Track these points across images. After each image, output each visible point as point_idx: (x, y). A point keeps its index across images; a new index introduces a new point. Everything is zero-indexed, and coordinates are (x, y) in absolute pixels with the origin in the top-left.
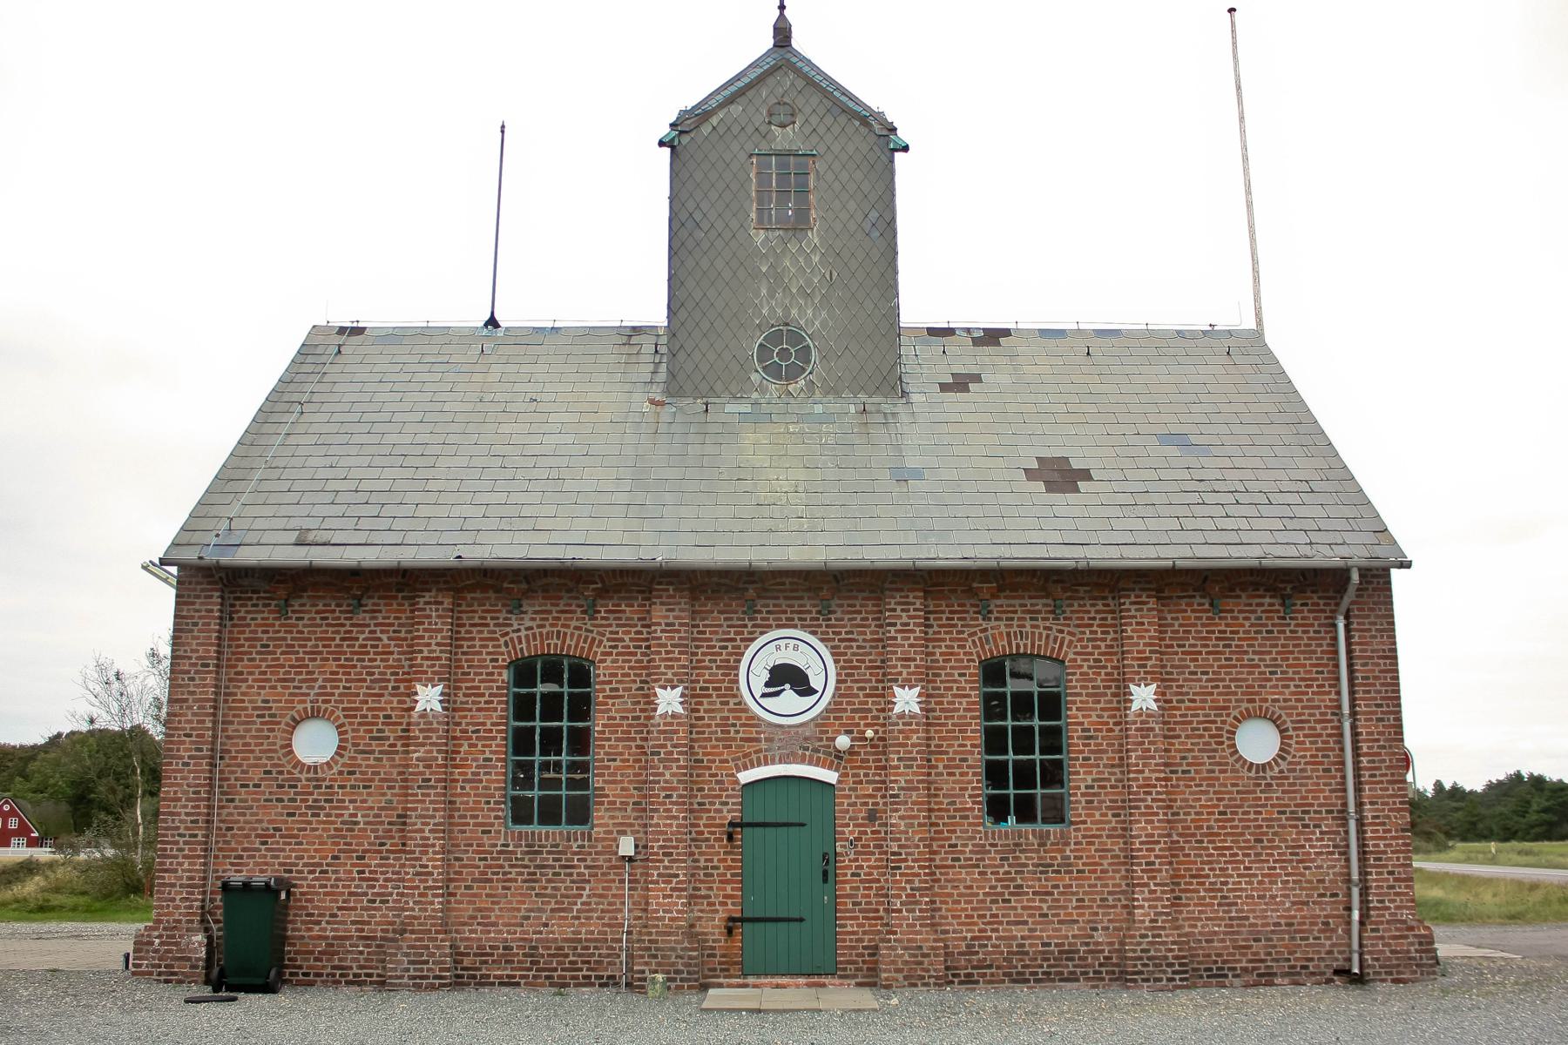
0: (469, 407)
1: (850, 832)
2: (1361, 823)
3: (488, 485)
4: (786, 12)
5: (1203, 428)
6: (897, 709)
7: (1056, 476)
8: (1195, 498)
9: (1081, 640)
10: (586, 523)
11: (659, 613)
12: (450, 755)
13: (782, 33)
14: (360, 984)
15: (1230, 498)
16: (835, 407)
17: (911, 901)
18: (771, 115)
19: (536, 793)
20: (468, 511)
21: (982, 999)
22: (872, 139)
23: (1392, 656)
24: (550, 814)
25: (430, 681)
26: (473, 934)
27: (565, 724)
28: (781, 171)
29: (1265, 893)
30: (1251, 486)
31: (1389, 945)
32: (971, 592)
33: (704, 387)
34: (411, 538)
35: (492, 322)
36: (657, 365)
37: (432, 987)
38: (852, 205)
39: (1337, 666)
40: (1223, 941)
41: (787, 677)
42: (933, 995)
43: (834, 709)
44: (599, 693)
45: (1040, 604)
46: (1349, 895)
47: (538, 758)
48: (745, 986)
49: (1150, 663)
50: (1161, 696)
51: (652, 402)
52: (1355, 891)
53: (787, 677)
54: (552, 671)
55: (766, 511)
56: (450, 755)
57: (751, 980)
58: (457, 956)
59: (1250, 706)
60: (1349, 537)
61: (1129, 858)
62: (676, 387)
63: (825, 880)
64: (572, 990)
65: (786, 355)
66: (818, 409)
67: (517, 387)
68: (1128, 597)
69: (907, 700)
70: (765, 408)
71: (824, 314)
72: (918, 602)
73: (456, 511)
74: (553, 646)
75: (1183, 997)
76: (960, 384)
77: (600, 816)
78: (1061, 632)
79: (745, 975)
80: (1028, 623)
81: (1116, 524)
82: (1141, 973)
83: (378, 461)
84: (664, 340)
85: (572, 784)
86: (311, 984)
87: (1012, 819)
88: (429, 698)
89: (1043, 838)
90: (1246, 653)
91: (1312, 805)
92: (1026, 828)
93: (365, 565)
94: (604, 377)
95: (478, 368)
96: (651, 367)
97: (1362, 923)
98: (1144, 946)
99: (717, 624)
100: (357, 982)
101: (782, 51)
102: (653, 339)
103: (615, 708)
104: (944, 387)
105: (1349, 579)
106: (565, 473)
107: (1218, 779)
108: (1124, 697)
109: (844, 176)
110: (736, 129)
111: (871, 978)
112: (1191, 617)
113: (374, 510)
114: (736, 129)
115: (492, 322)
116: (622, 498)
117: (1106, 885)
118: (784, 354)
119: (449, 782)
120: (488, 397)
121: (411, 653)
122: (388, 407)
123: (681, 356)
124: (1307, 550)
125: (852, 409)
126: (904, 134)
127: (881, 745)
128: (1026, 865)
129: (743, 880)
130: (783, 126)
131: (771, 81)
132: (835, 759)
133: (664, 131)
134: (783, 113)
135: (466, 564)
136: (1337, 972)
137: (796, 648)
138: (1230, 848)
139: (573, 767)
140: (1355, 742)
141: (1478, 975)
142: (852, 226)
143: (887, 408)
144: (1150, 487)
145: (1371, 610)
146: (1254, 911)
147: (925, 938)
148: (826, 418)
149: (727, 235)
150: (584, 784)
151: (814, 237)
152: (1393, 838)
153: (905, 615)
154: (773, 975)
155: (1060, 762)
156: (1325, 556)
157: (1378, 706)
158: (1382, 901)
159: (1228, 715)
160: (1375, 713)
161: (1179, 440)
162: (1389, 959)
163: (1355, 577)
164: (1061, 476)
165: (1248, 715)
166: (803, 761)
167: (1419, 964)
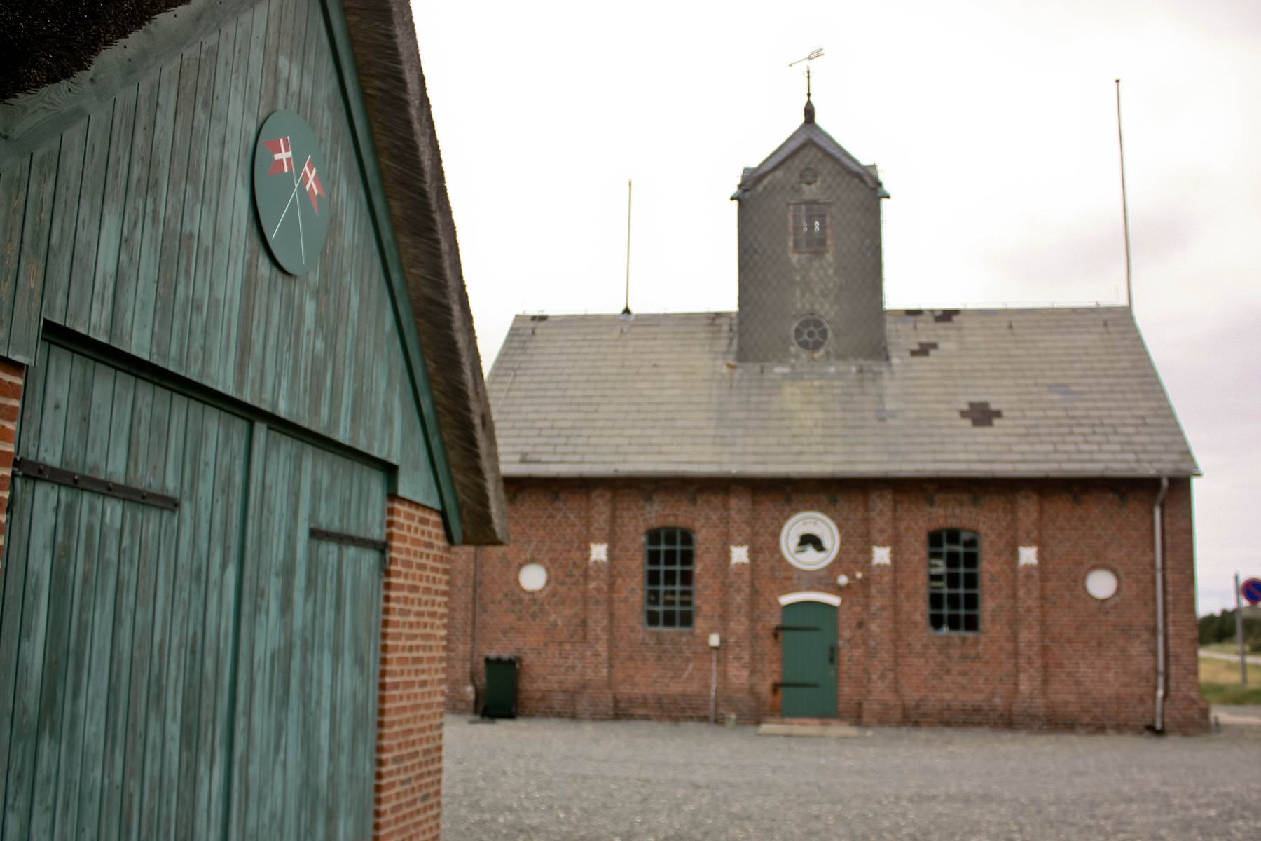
0: (615, 371)
1: (846, 634)
4: (812, 98)
8: (1065, 430)
11: (734, 503)
12: (612, 586)
13: (809, 112)
16: (843, 368)
20: (619, 441)
21: (923, 734)
24: (669, 620)
26: (625, 690)
28: (809, 207)
29: (1099, 677)
30: (1106, 421)
34: (587, 458)
35: (627, 311)
43: (838, 561)
44: (698, 548)
45: (965, 497)
51: (730, 366)
54: (670, 538)
55: (797, 440)
56: (612, 586)
58: (616, 702)
60: (1164, 457)
61: (1016, 654)
62: (743, 355)
63: (832, 660)
65: (812, 335)
66: (832, 369)
67: (646, 356)
69: (882, 555)
70: (799, 369)
74: (671, 521)
75: (1042, 739)
76: (924, 350)
77: (700, 623)
83: (564, 408)
84: (735, 322)
85: (683, 603)
88: (599, 552)
89: (964, 640)
92: (955, 634)
99: (768, 509)
100: (559, 715)
104: (914, 353)
108: (1015, 555)
112: (1060, 509)
113: (563, 440)
115: (627, 311)
116: (711, 432)
118: (811, 334)
119: (611, 602)
121: (588, 525)
124: (1134, 465)
125: (854, 369)
126: (887, 187)
130: (809, 183)
131: (801, 154)
132: (838, 590)
133: (734, 190)
134: (808, 175)
139: (683, 593)
141: (1240, 733)
143: (876, 368)
147: (890, 698)
148: (840, 376)
150: (689, 603)
151: (829, 257)
153: (881, 506)
156: (1148, 469)
161: (1063, 389)
163: (1165, 483)
164: (982, 415)
167: (1193, 723)
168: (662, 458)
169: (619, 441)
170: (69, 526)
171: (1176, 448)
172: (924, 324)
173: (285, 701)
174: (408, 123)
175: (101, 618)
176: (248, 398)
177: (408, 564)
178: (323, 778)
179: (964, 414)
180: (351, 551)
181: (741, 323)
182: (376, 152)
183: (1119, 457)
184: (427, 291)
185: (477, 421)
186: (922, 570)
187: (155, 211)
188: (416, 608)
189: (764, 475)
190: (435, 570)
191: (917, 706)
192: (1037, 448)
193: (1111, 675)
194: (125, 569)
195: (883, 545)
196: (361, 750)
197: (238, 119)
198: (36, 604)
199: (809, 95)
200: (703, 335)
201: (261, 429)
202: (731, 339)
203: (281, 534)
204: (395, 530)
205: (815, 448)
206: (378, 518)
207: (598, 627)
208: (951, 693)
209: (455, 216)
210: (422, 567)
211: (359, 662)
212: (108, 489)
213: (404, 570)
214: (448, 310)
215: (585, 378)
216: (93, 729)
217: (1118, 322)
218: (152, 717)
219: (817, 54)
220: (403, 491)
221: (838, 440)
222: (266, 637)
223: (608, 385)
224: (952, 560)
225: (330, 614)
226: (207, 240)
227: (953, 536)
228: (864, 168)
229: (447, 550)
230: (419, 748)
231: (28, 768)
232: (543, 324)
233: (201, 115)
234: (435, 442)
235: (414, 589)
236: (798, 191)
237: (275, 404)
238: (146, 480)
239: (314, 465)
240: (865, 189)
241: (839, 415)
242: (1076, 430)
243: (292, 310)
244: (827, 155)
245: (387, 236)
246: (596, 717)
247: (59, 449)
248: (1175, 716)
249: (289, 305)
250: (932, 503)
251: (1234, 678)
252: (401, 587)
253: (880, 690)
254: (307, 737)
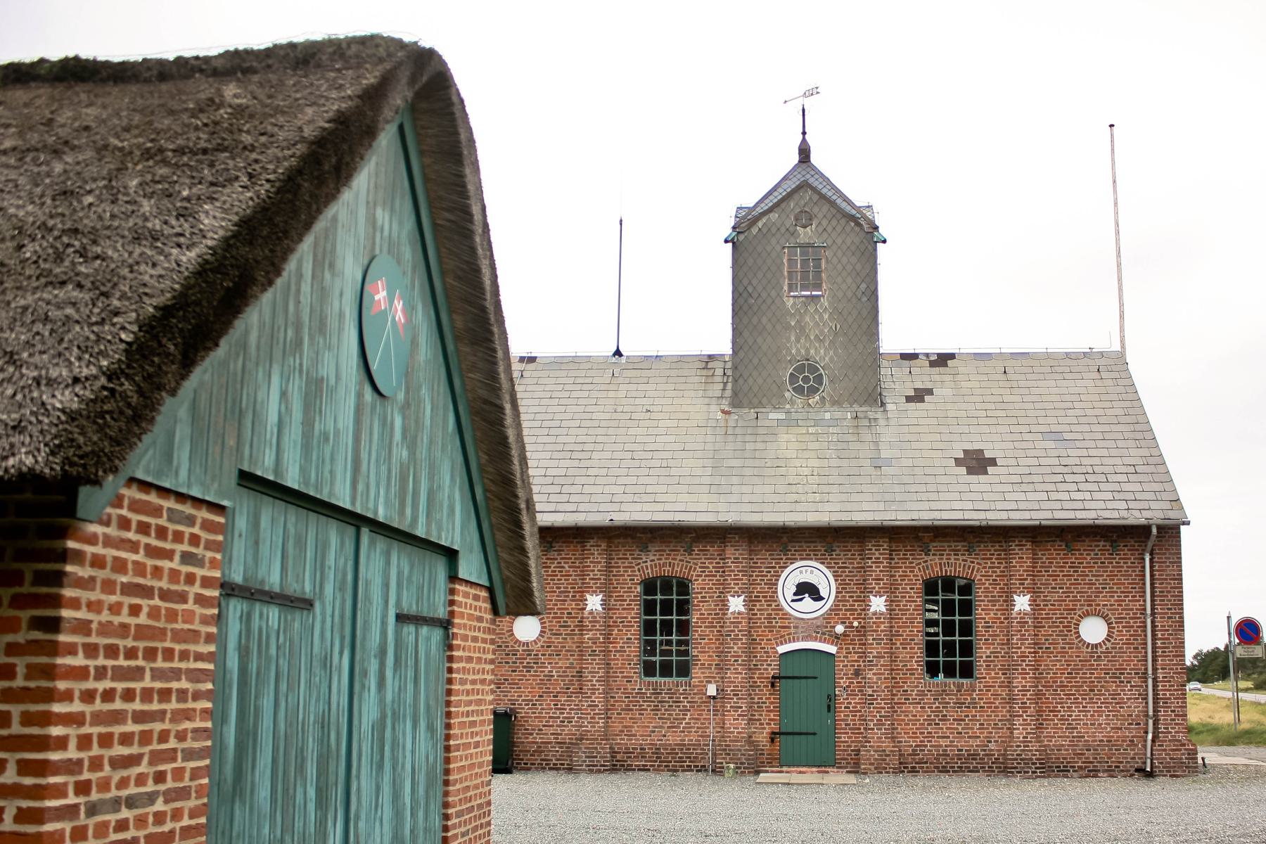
0: (608, 416)
1: (843, 682)
2: (1155, 680)
3: (624, 471)
5: (1074, 428)
6: (872, 610)
7: (974, 463)
8: (1060, 478)
10: (686, 497)
11: (730, 552)
12: (607, 636)
13: (804, 152)
14: (557, 769)
15: (1082, 478)
16: (838, 415)
17: (880, 724)
18: (797, 220)
19: (657, 658)
20: (614, 489)
21: (920, 781)
22: (862, 234)
23: (1179, 579)
24: (666, 670)
26: (622, 740)
27: (674, 617)
28: (802, 250)
29: (1094, 723)
32: (918, 539)
33: (755, 401)
35: (618, 353)
36: (725, 384)
37: (599, 771)
38: (849, 280)
39: (1144, 584)
41: (807, 589)
42: (892, 778)
43: (835, 609)
45: (960, 545)
46: (1147, 724)
47: (658, 638)
50: (1033, 602)
51: (723, 412)
52: (1151, 722)
53: (807, 589)
55: (794, 488)
56: (607, 636)
57: (785, 769)
58: (613, 753)
60: (1154, 505)
61: (1011, 700)
63: (829, 710)
64: (680, 773)
65: (807, 380)
66: (828, 416)
67: (638, 401)
69: (878, 604)
70: (794, 416)
71: (831, 352)
73: (607, 489)
74: (667, 571)
75: (1037, 783)
76: (919, 396)
77: (696, 672)
80: (953, 557)
81: (1008, 497)
83: (556, 455)
84: (729, 365)
85: (679, 653)
86: (529, 769)
87: (941, 675)
88: (594, 602)
89: (959, 687)
92: (951, 680)
93: (556, 525)
94: (692, 394)
95: (612, 387)
96: (721, 386)
97: (1153, 741)
99: (764, 558)
100: (555, 768)
101: (804, 166)
102: (722, 365)
103: (704, 608)
104: (909, 399)
105: (1151, 532)
106: (671, 463)
108: (1010, 603)
109: (844, 260)
110: (774, 230)
111: (855, 769)
113: (557, 489)
114: (774, 230)
115: (618, 353)
116: (707, 480)
118: (806, 379)
119: (607, 652)
120: (620, 409)
121: (583, 575)
122: (557, 417)
123: (741, 381)
124: (1124, 514)
126: (884, 231)
127: (862, 631)
129: (781, 710)
130: (804, 227)
131: (796, 196)
132: (836, 639)
133: (727, 231)
134: (805, 218)
135: (616, 523)
136: (1137, 770)
137: (812, 572)
139: (679, 643)
140: (1153, 631)
141: (1225, 774)
142: (849, 294)
144: (1033, 470)
147: (887, 745)
148: (835, 422)
149: (769, 301)
150: (686, 653)
153: (877, 553)
154: (798, 766)
155: (971, 641)
161: (1056, 436)
163: (1154, 530)
164: (977, 463)
165: (1087, 614)
166: (816, 639)
167: (1184, 766)
168: (659, 507)
169: (614, 489)
170: (249, 631)
171: (1165, 496)
172: (921, 367)
173: (380, 766)
174: (473, 250)
175: (267, 703)
176: (358, 510)
177: (465, 638)
178: (407, 832)
179: (958, 462)
180: (424, 630)
181: (735, 368)
182: (443, 273)
183: (1110, 505)
184: (483, 393)
185: (523, 506)
186: (917, 615)
187: (301, 365)
188: (471, 677)
189: (761, 524)
190: (484, 641)
191: (914, 753)
192: (1031, 496)
193: (1102, 720)
194: (281, 661)
195: (879, 594)
196: (432, 806)
197: (350, 269)
198: (230, 698)
199: (804, 133)
200: (697, 379)
201: (365, 531)
202: (725, 384)
203: (378, 623)
204: (456, 608)
205: (811, 497)
206: (442, 598)
207: (594, 676)
208: (948, 739)
209: (507, 325)
210: (475, 639)
211: (431, 728)
212: (270, 598)
213: (463, 644)
214: (501, 409)
215: (577, 423)
216: (264, 793)
217: (1109, 368)
218: (299, 783)
219: (812, 92)
220: (462, 574)
221: (835, 489)
222: (368, 712)
223: (600, 431)
224: (948, 608)
225: (410, 687)
226: (332, 382)
227: (949, 584)
228: (858, 209)
229: (493, 622)
230: (474, 803)
231: (228, 826)
232: (531, 366)
233: (327, 275)
234: (485, 526)
235: (470, 659)
236: (794, 234)
237: (376, 512)
238: (293, 588)
239: (401, 559)
240: (862, 233)
241: (834, 463)
242: (1069, 478)
243: (387, 426)
244: (823, 197)
245: (451, 347)
246: (593, 770)
247: (242, 569)
248: (1161, 756)
249: (384, 423)
250: (689, 551)
251: (1226, 718)
252: (460, 659)
253: (878, 738)
254: (396, 796)
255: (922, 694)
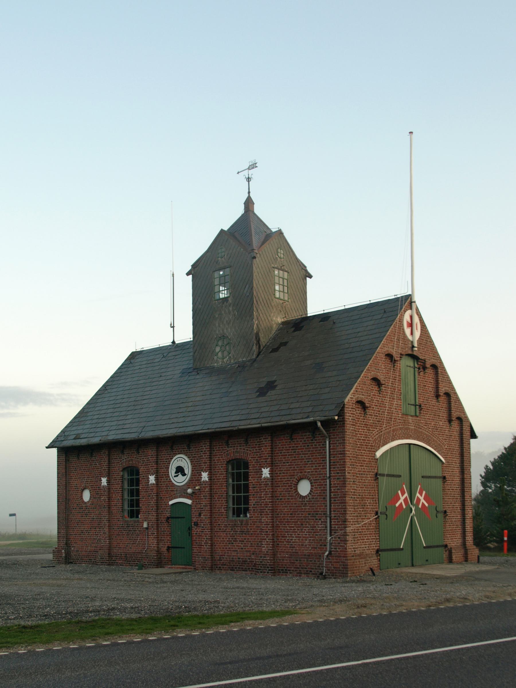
9: (253, 453)
13: (249, 203)
25: (104, 477)
31: (333, 565)
35: (174, 342)
40: (287, 560)
41: (180, 470)
48: (172, 568)
49: (268, 460)
53: (180, 470)
57: (173, 566)
59: (301, 474)
63: (189, 535)
68: (262, 436)
72: (208, 443)
78: (247, 450)
79: (172, 565)
82: (260, 569)
90: (300, 454)
91: (319, 511)
98: (261, 561)
107: (290, 502)
115: (174, 342)
117: (258, 539)
128: (237, 531)
138: (293, 527)
145: (337, 435)
146: (300, 550)
152: (341, 525)
153: (205, 446)
157: (338, 473)
158: (336, 549)
159: (294, 478)
160: (337, 476)
162: (333, 570)
199: (249, 193)
219: (253, 166)
250: (123, 453)
255: (226, 526)
